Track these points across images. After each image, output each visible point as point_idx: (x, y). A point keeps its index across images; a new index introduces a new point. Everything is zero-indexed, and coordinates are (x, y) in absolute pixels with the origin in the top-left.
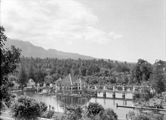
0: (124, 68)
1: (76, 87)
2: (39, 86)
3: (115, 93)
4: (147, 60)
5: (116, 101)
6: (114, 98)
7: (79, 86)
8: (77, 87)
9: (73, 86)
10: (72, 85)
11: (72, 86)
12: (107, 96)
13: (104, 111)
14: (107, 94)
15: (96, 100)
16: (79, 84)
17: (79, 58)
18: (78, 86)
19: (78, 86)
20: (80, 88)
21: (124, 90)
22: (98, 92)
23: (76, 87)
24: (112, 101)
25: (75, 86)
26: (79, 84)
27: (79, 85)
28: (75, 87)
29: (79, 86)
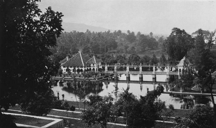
0: (148, 42)
1: (89, 68)
2: (107, 70)
3: (155, 75)
4: (140, 32)
5: (145, 86)
6: (141, 81)
7: (94, 66)
8: (90, 69)
9: (85, 67)
10: (84, 65)
11: (83, 67)
12: (144, 80)
13: (88, 106)
14: (131, 76)
15: (117, 84)
16: (94, 65)
17: (88, 30)
18: (91, 67)
19: (91, 67)
20: (94, 69)
21: (107, 70)
22: (118, 74)
23: (89, 68)
24: (138, 85)
25: (87, 67)
26: (94, 65)
27: (93, 65)
28: (87, 69)
29: (93, 67)
